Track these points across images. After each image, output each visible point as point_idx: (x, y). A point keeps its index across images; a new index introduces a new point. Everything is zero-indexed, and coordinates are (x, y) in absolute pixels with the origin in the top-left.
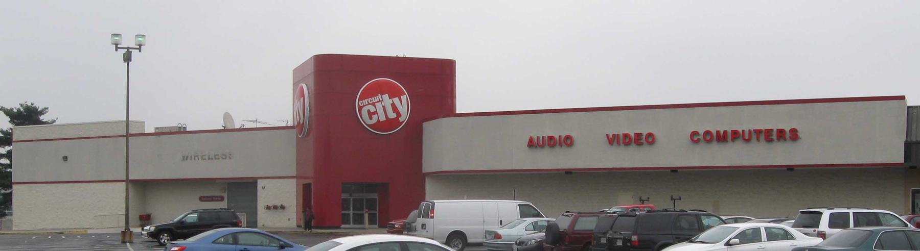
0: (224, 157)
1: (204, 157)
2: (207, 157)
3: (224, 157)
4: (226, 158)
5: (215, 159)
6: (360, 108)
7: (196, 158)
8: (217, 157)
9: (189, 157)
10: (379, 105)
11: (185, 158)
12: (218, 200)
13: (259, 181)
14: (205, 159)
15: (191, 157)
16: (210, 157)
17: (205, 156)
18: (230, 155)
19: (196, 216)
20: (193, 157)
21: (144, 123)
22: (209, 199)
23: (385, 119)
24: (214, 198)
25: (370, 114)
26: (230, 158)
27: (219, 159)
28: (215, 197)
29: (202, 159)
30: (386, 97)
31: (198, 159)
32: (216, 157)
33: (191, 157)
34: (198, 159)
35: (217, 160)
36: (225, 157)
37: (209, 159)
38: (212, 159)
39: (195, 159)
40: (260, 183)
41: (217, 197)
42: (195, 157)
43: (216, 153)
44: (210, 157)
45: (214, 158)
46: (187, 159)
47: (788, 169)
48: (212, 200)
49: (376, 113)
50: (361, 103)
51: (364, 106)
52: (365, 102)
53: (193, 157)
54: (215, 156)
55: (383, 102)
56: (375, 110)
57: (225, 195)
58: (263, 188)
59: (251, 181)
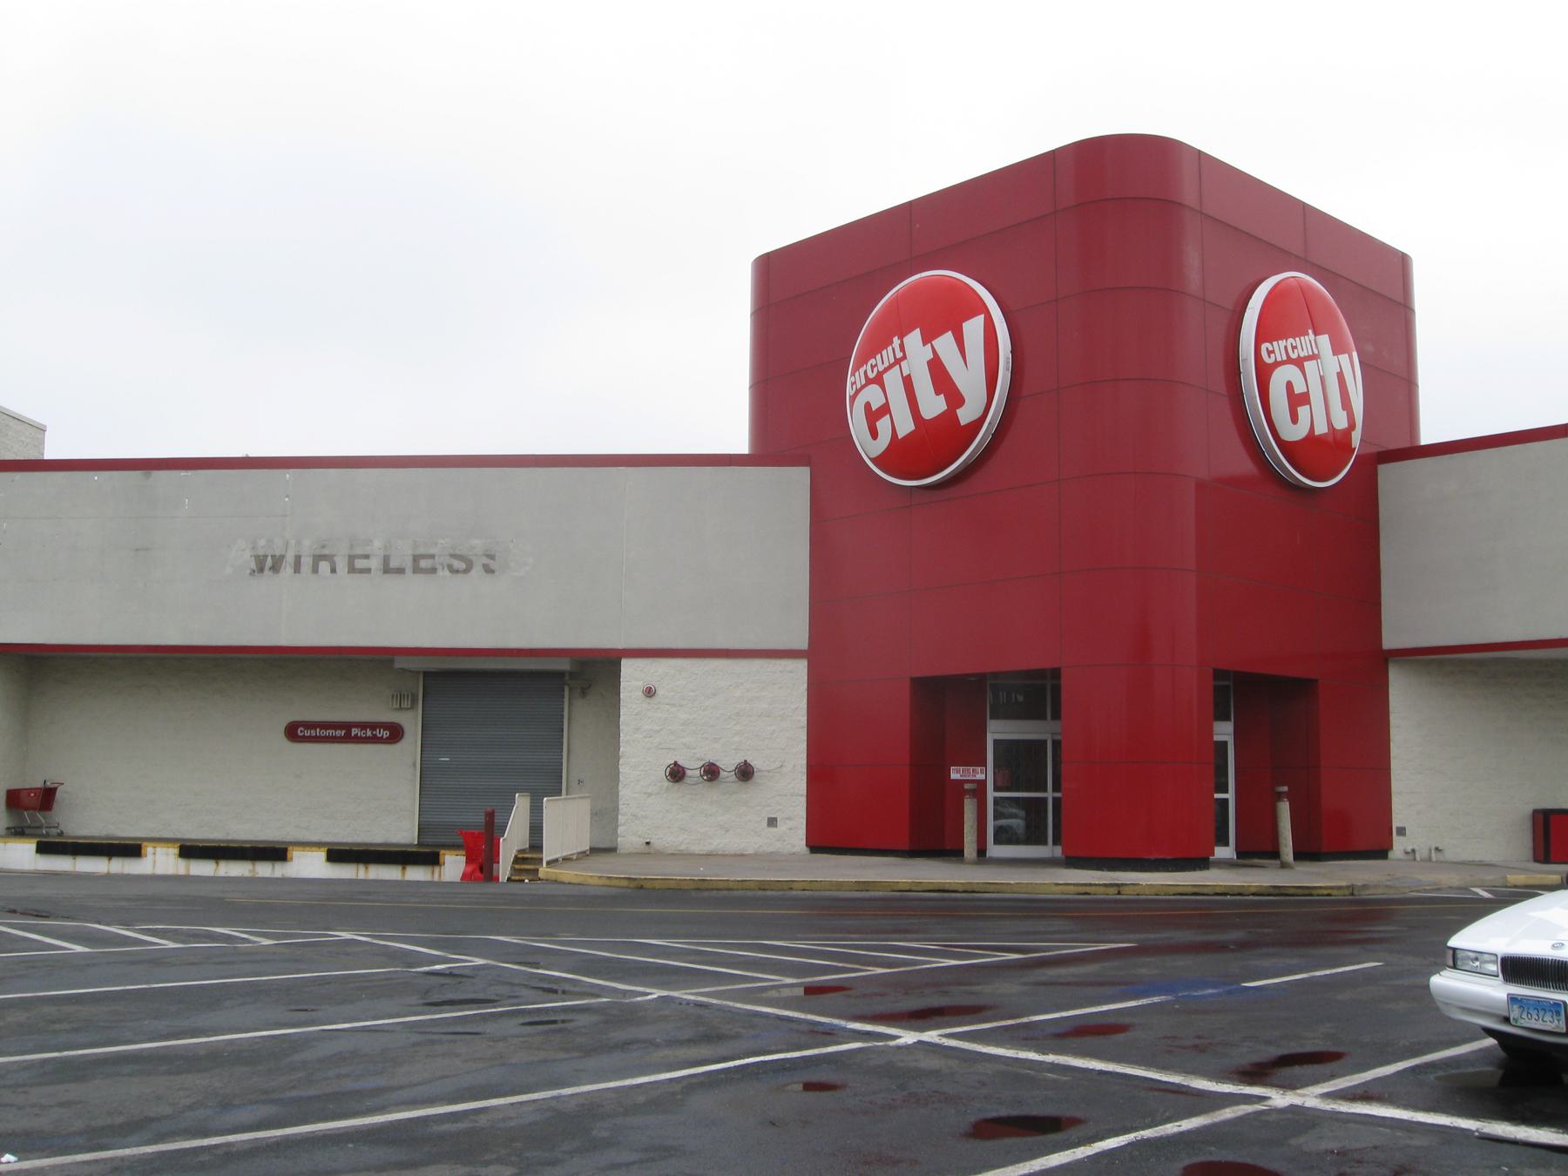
0: (457, 564)
1: (360, 564)
2: (375, 563)
3: (457, 564)
4: (467, 571)
5: (417, 570)
6: (1264, 373)
7: (324, 566)
8: (423, 564)
9: (290, 558)
10: (893, 379)
11: (268, 564)
12: (375, 740)
13: (628, 667)
14: (368, 571)
15: (298, 559)
16: (393, 564)
17: (367, 557)
18: (492, 557)
19: (25, 813)
20: (307, 562)
21: (42, 430)
22: (330, 732)
23: (1326, 431)
24: (354, 731)
25: (1297, 400)
26: (488, 570)
27: (433, 570)
28: (363, 726)
29: (352, 569)
30: (914, 339)
31: (333, 571)
32: (421, 565)
33: (298, 559)
34: (333, 571)
35: (421, 577)
36: (462, 564)
37: (387, 570)
38: (401, 571)
39: (315, 570)
40: (632, 674)
41: (373, 726)
42: (318, 558)
43: (421, 551)
44: (393, 564)
45: (409, 570)
46: (275, 568)
47: (539, 963)
48: (348, 739)
49: (885, 409)
50: (1270, 353)
51: (1277, 364)
52: (1277, 349)
53: (307, 562)
54: (416, 559)
55: (904, 364)
56: (1306, 390)
57: (412, 723)
58: (650, 693)
59: (564, 665)
